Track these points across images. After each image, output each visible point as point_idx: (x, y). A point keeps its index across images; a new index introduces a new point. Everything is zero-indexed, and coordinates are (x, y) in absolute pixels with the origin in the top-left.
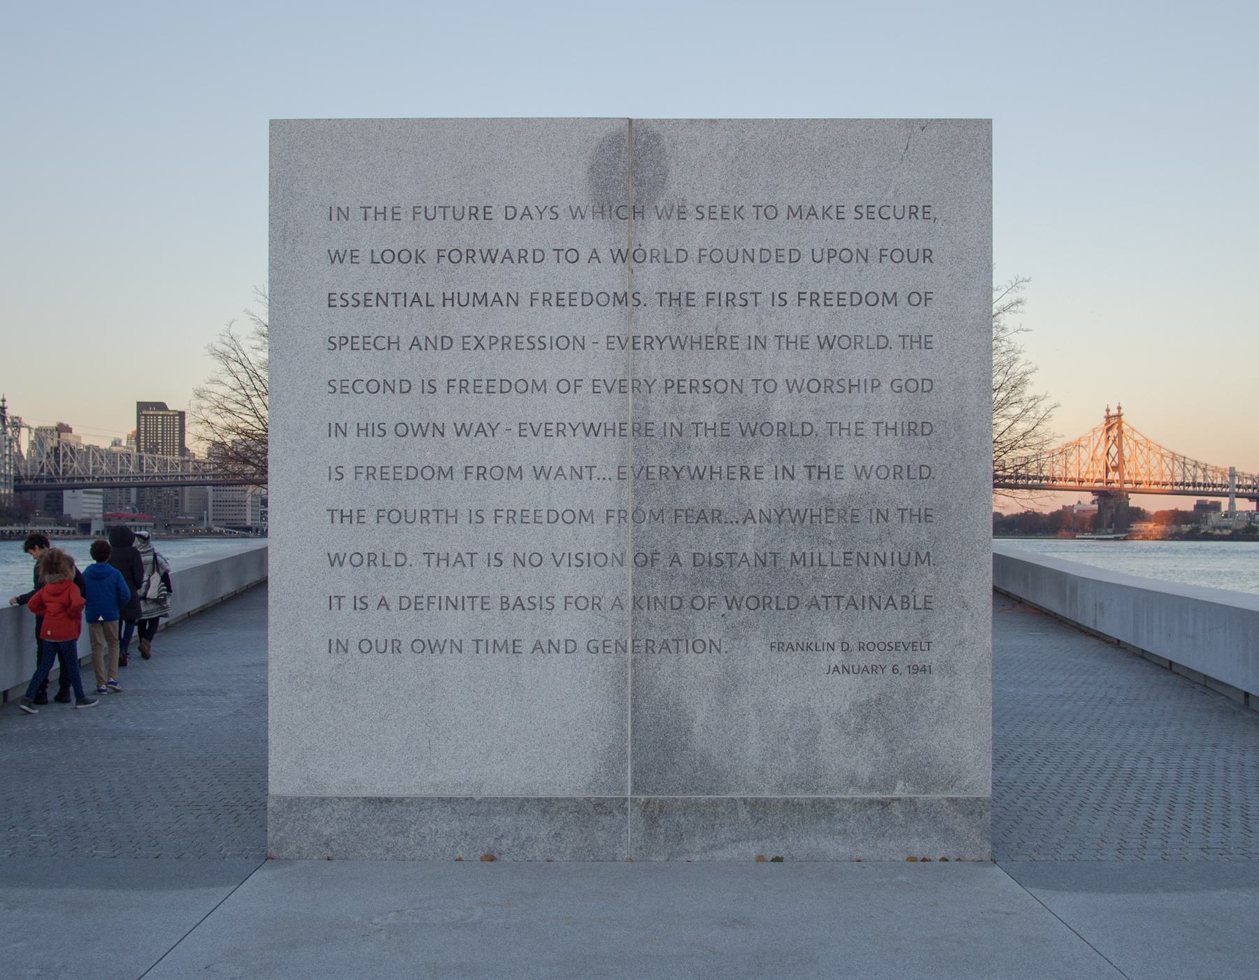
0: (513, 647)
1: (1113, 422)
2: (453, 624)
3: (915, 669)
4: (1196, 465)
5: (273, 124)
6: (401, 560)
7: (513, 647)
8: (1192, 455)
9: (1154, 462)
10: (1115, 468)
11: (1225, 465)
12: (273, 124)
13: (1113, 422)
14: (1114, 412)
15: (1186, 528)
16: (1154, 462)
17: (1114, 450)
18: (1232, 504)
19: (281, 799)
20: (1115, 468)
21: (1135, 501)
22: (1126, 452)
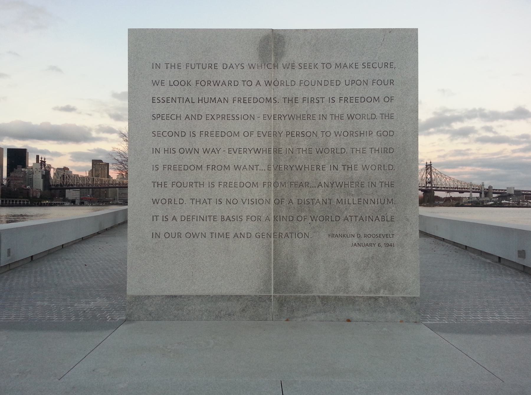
0: (227, 236)
2: (201, 227)
7: (227, 236)
9: (443, 180)
10: (429, 183)
14: (429, 163)
17: (429, 176)
21: (437, 194)
22: (433, 176)
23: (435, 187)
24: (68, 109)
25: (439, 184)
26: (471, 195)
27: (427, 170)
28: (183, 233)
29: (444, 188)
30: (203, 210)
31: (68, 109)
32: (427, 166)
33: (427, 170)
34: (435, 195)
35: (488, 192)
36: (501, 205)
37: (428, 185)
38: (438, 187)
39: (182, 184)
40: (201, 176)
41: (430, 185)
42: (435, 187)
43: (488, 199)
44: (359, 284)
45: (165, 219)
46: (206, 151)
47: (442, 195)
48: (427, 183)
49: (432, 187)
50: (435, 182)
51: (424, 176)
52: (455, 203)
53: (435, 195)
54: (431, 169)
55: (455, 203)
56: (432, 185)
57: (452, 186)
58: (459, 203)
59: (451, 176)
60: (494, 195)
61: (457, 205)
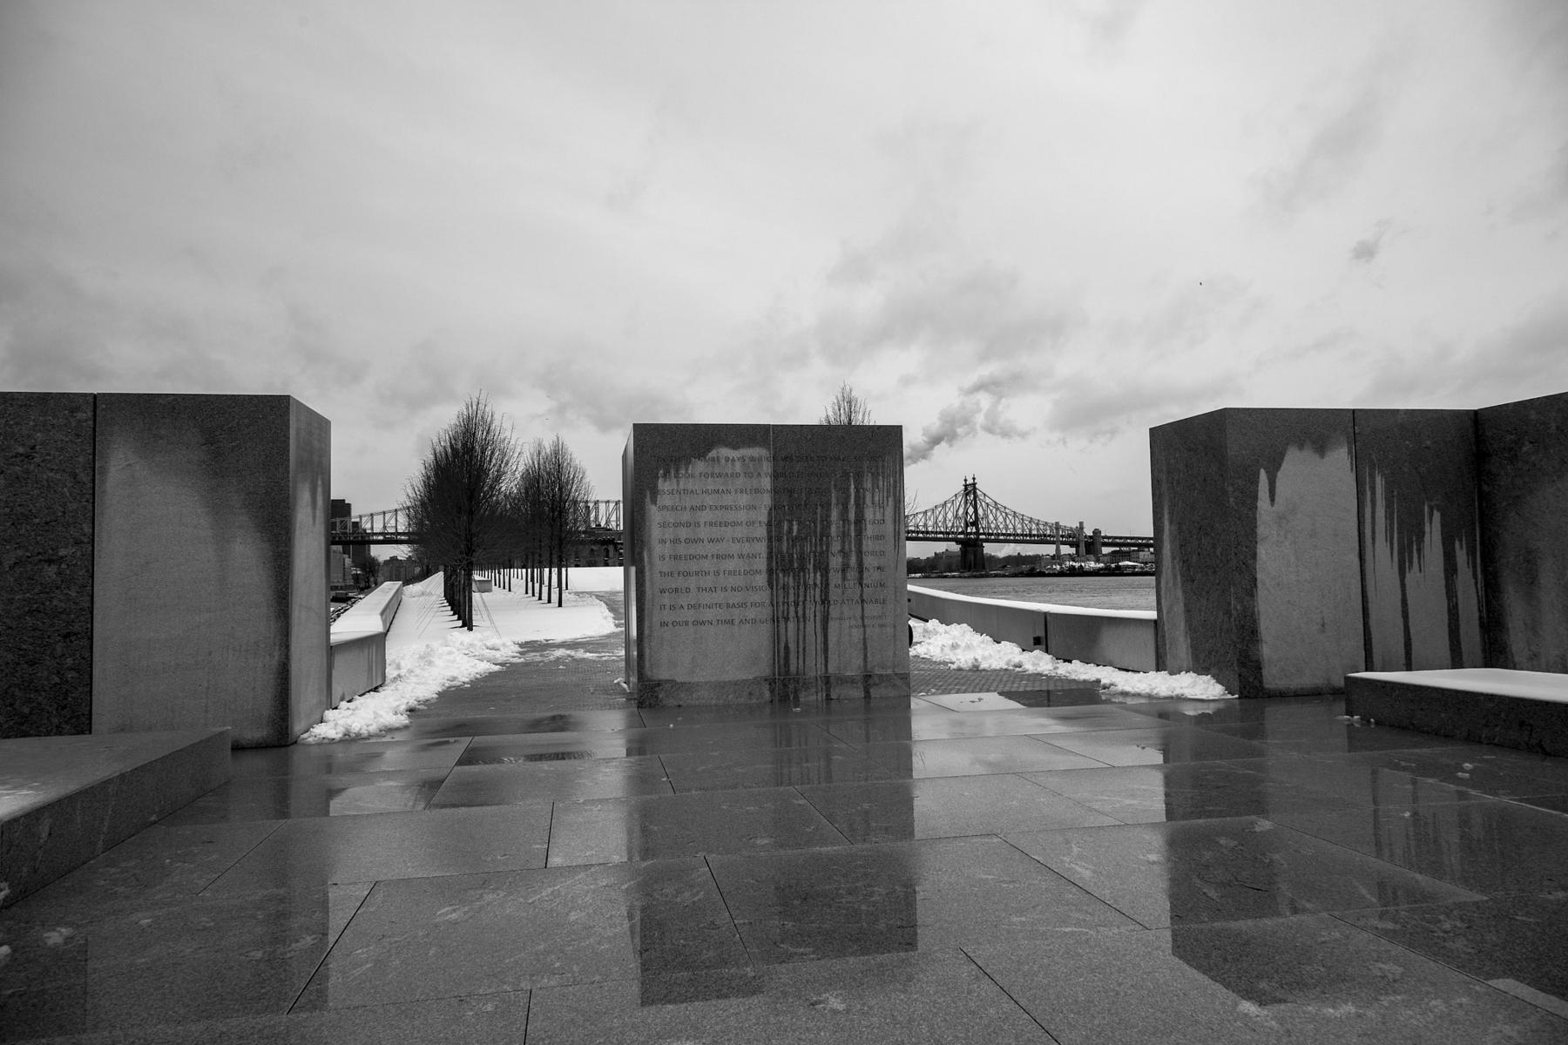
0: (732, 622)
1: (970, 490)
2: (708, 615)
3: (881, 626)
4: (1031, 520)
5: (900, 427)
6: (688, 590)
7: (732, 622)
8: (1029, 513)
9: (1001, 519)
10: (973, 524)
11: (1052, 521)
12: (900, 427)
13: (970, 490)
14: (970, 481)
15: (1025, 568)
16: (1001, 519)
17: (971, 510)
18: (1058, 550)
19: (913, 448)
20: (973, 524)
21: (990, 549)
22: (980, 512)
26: (1058, 550)
28: (691, 620)
30: (706, 598)
34: (986, 551)
35: (1090, 544)
36: (1119, 572)
39: (689, 574)
40: (706, 565)
44: (864, 548)
45: (672, 607)
46: (711, 541)
48: (967, 525)
49: (977, 533)
51: (961, 511)
55: (1010, 569)
60: (1106, 550)
61: (1032, 573)
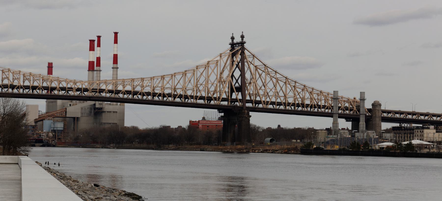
9: (270, 85)
10: (239, 89)
14: (238, 39)
17: (237, 73)
22: (248, 75)
23: (250, 101)
24: (359, 189)
25: (261, 92)
26: (335, 123)
27: (233, 55)
29: (273, 103)
31: (359, 189)
32: (233, 45)
33: (233, 55)
34: (350, 123)
35: (365, 116)
37: (234, 96)
38: (260, 102)
41: (240, 97)
42: (250, 101)
43: (372, 134)
47: (139, 117)
48: (232, 91)
49: (243, 100)
50: (251, 89)
51: (226, 73)
52: (298, 143)
53: (350, 123)
54: (243, 54)
56: (244, 95)
57: (291, 100)
58: (310, 144)
59: (292, 75)
60: (386, 126)
61: (307, 151)
